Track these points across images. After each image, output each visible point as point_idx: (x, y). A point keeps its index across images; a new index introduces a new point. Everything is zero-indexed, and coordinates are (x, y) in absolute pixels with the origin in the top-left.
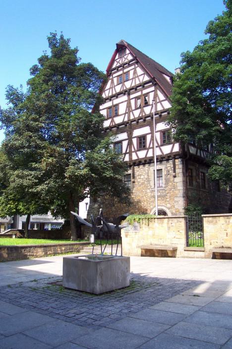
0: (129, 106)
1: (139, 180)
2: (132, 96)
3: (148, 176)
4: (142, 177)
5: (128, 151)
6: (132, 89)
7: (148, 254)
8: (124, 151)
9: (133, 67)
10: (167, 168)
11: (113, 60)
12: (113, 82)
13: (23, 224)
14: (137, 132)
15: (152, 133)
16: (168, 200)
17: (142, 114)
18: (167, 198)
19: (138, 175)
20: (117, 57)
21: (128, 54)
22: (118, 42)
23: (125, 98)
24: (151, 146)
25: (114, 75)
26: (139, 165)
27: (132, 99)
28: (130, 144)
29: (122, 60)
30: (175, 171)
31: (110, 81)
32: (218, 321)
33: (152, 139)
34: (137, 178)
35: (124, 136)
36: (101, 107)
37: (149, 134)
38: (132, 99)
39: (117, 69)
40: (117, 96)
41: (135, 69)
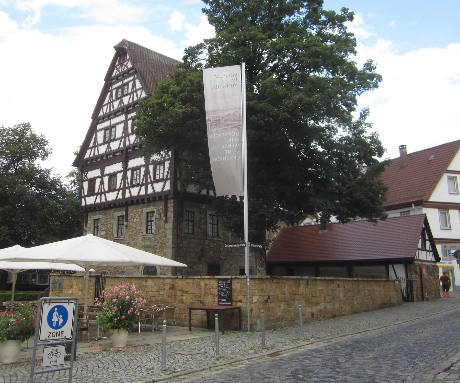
0: (125, 129)
1: (131, 224)
2: (130, 116)
3: (141, 219)
4: (135, 220)
5: (122, 187)
6: (111, 114)
7: (36, 281)
8: (96, 191)
9: (132, 78)
10: (159, 210)
11: (112, 67)
12: (111, 96)
13: (214, 329)
14: (109, 170)
15: (147, 166)
16: (157, 251)
17: (137, 141)
18: (156, 249)
19: (131, 218)
20: (117, 63)
21: (128, 60)
22: (117, 42)
23: (122, 118)
24: (144, 182)
25: (114, 86)
26: (92, 211)
27: (100, 130)
29: (122, 67)
30: (166, 216)
31: (109, 94)
32: (105, 350)
33: (102, 183)
34: (130, 221)
35: (118, 167)
36: (99, 127)
37: (142, 166)
38: (100, 130)
39: (117, 79)
40: (115, 114)
41: (134, 80)
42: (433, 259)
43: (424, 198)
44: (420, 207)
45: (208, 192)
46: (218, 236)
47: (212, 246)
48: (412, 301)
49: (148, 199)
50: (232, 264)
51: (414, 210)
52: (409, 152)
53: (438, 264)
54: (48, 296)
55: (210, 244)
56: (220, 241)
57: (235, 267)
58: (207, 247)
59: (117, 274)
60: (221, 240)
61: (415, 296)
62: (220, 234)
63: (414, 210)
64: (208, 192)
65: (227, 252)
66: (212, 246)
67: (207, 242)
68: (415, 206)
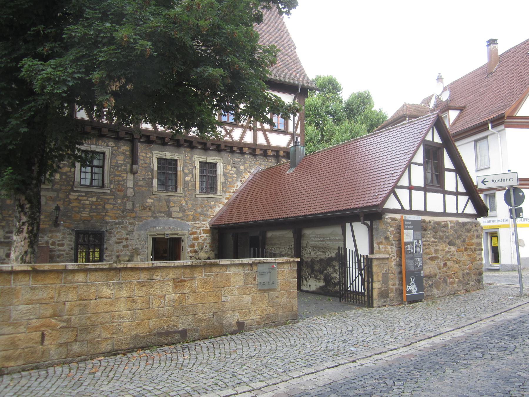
42: (471, 209)
43: (507, 112)
44: (502, 127)
45: (255, 137)
46: (103, 186)
47: (87, 202)
48: (370, 305)
50: (133, 231)
51: (494, 133)
52: (502, 48)
53: (481, 220)
54: (178, 258)
55: (80, 198)
56: (105, 194)
57: (139, 235)
58: (74, 204)
59: (468, 222)
60: (109, 191)
61: (375, 293)
62: (106, 181)
63: (494, 133)
64: (255, 137)
65: (123, 212)
66: (87, 202)
67: (73, 196)
68: (493, 127)
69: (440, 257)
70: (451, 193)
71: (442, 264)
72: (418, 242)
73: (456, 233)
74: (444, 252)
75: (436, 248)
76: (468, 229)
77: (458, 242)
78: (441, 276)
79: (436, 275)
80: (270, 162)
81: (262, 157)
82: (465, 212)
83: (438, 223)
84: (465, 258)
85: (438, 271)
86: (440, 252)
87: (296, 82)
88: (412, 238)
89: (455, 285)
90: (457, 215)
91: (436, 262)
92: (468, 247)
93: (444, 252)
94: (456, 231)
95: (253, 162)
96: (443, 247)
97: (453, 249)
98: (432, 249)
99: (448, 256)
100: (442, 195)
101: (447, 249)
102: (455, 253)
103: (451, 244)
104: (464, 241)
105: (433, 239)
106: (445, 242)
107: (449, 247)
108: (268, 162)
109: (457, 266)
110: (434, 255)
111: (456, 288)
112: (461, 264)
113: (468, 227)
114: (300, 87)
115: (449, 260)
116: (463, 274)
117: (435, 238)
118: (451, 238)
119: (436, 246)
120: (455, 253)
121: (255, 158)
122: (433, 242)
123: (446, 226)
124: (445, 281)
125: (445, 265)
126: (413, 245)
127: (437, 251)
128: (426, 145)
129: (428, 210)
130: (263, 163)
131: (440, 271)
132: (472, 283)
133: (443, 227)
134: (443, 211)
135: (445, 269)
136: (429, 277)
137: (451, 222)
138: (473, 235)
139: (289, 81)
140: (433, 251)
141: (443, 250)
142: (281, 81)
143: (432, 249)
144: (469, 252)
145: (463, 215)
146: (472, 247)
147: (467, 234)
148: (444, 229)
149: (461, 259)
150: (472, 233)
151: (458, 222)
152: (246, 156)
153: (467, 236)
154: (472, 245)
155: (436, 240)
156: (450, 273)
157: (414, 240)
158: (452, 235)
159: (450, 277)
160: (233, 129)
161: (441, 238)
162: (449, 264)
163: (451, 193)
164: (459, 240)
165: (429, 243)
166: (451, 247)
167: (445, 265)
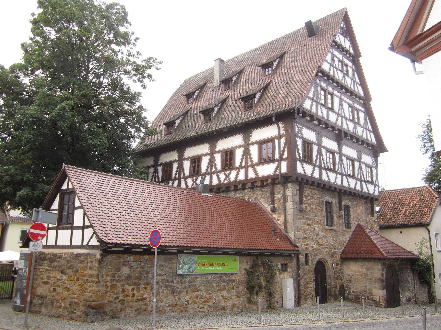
28: (247, 153)
49: (297, 178)
69: (51, 282)
70: (78, 228)
71: (52, 289)
72: (26, 269)
73: (68, 263)
74: (56, 279)
75: (48, 275)
76: (80, 260)
77: (69, 272)
78: (50, 298)
79: (46, 297)
80: (267, 191)
81: (259, 188)
82: (89, 244)
83: (55, 255)
84: (76, 288)
85: (48, 294)
86: (52, 279)
87: (268, 114)
88: (23, 265)
89: (61, 310)
90: (71, 247)
91: (48, 286)
92: (80, 277)
93: (56, 279)
94: (68, 261)
95: (251, 195)
96: (55, 275)
97: (64, 277)
98: (45, 276)
99: (59, 283)
100: (69, 231)
101: (59, 277)
102: (66, 281)
103: (62, 272)
104: (77, 271)
105: (48, 268)
106: (58, 270)
107: (61, 275)
108: (264, 191)
109: (66, 293)
110: (46, 280)
111: (61, 313)
112: (70, 292)
113: (81, 258)
114: (274, 115)
115: (59, 287)
116: (70, 302)
117: (50, 267)
118: (63, 268)
119: (49, 273)
120: (66, 281)
121: (254, 191)
122: (47, 270)
123: (60, 257)
124: (52, 303)
125: (54, 290)
126: (22, 270)
127: (49, 277)
128: (304, 141)
129: (58, 244)
130: (260, 193)
131: (50, 294)
132: (79, 314)
133: (59, 258)
134: (81, 244)
135: (54, 293)
136: (41, 297)
137: (65, 254)
138: (86, 267)
139: (264, 115)
140: (45, 277)
141: (54, 277)
142: (264, 117)
143: (45, 276)
144: (81, 282)
145: (88, 247)
146: (84, 278)
147: (80, 265)
148: (59, 260)
149: (71, 288)
150: (85, 264)
151: (72, 253)
152: (246, 191)
153: (80, 267)
154: (85, 276)
155: (50, 269)
156: (58, 298)
157: (24, 267)
158: (64, 265)
159: (58, 301)
160: (230, 172)
161: (55, 267)
162: (59, 290)
163: (78, 228)
164: (70, 270)
165: (44, 270)
166: (63, 275)
167: (54, 290)
